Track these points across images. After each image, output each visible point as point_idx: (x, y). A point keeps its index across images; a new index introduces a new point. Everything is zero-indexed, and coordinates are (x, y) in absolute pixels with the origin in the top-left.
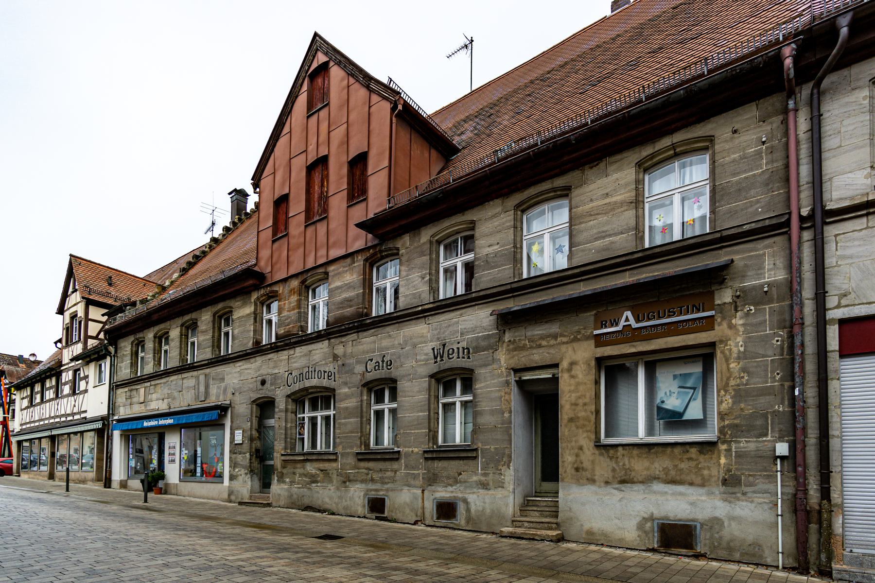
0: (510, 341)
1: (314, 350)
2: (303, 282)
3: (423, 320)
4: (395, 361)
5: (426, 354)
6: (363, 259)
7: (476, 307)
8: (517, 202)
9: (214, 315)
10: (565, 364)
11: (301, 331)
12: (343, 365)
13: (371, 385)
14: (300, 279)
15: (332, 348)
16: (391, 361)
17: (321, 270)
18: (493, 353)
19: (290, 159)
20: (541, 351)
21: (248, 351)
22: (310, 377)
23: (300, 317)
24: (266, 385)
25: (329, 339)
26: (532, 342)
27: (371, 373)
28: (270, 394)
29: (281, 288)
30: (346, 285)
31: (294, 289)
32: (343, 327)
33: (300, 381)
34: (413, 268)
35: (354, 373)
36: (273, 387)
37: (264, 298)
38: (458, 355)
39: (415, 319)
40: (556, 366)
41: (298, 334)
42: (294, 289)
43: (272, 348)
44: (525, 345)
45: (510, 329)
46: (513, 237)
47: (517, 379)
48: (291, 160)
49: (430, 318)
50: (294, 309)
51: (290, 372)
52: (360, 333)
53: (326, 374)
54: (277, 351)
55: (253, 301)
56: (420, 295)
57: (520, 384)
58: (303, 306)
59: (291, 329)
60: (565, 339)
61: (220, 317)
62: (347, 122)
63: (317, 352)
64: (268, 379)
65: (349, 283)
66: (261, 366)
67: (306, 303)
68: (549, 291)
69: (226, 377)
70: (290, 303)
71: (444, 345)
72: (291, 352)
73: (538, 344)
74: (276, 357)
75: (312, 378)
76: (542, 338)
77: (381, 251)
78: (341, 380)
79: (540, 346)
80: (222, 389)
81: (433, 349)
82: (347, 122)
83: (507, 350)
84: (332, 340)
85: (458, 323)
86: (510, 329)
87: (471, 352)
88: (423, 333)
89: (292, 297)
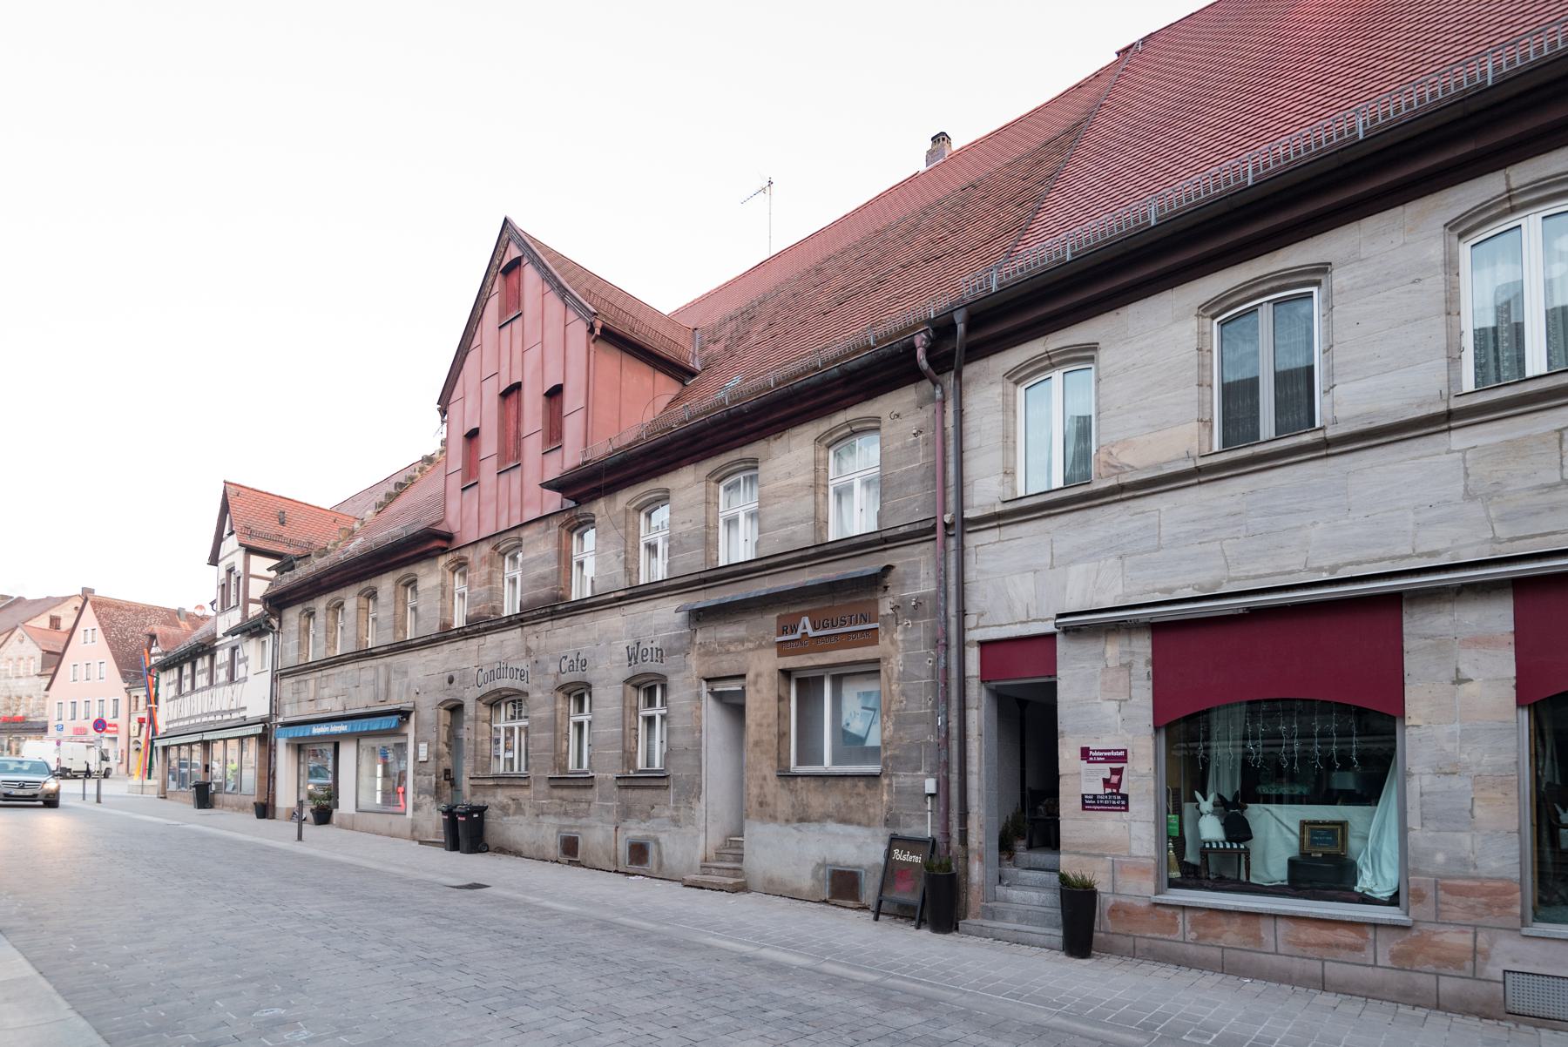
0: (701, 644)
5: (621, 654)
7: (670, 598)
10: (750, 676)
17: (514, 534)
20: (729, 658)
21: (433, 637)
27: (565, 675)
28: (458, 696)
29: (471, 554)
31: (485, 557)
36: (462, 687)
40: (743, 676)
42: (485, 557)
43: (460, 635)
47: (709, 690)
49: (625, 607)
51: (480, 668)
52: (555, 622)
53: (518, 673)
55: (440, 568)
57: (712, 693)
59: (481, 611)
60: (751, 645)
62: (542, 342)
63: (509, 643)
64: (456, 675)
65: (544, 555)
66: (448, 658)
67: (501, 576)
70: (481, 576)
71: (638, 644)
77: (577, 517)
79: (728, 652)
81: (628, 648)
83: (699, 654)
84: (525, 629)
85: (651, 616)
86: (701, 629)
89: (483, 567)
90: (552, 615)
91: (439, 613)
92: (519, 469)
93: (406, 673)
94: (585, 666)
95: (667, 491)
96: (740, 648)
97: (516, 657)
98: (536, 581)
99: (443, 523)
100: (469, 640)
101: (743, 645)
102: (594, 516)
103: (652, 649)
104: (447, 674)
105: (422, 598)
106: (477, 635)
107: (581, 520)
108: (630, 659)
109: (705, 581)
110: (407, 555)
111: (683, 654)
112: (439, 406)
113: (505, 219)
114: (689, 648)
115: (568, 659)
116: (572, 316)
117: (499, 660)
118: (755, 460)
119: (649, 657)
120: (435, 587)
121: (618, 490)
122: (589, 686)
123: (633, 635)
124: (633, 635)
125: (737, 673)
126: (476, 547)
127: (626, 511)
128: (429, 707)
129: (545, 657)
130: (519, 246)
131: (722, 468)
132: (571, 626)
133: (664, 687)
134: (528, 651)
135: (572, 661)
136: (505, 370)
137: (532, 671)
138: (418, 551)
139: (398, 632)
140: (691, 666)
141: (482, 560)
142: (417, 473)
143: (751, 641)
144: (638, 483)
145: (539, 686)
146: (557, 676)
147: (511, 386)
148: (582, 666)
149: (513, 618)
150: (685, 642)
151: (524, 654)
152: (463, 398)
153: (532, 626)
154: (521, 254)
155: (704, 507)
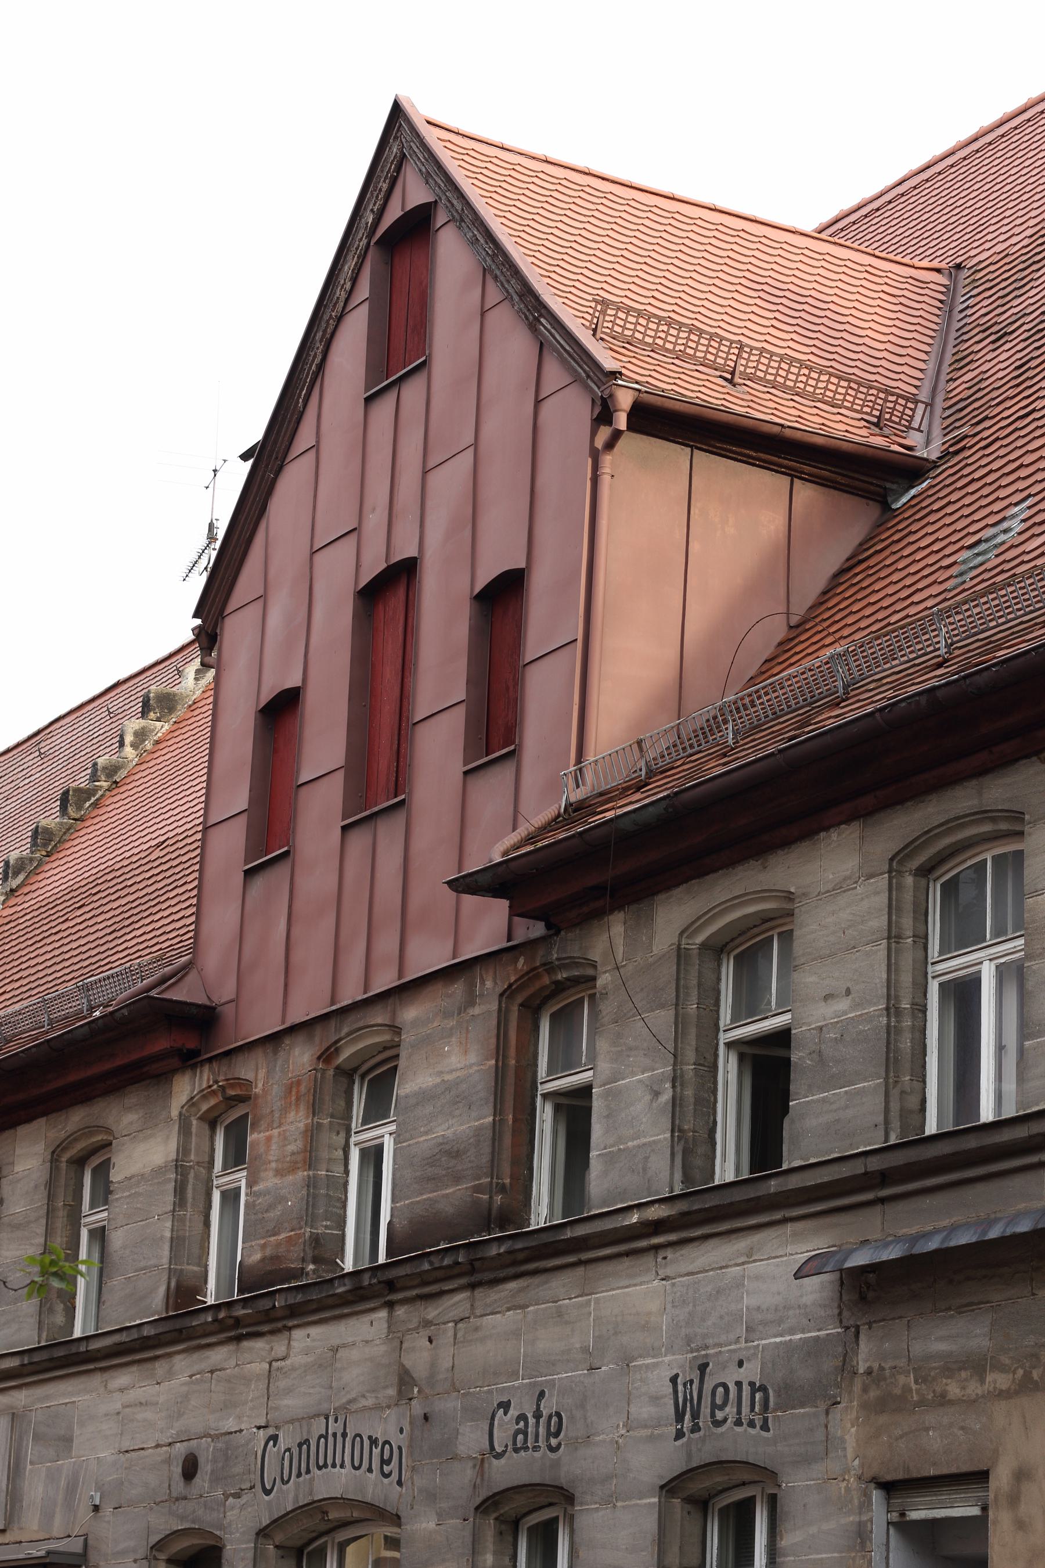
0: (869, 1372)
1: (344, 1346)
2: (327, 1056)
3: (648, 1260)
4: (572, 1418)
5: (655, 1399)
6: (499, 989)
7: (789, 1227)
8: (894, 846)
9: (54, 1159)
10: (1001, 1478)
11: (315, 1260)
12: (426, 1418)
13: (507, 1509)
14: (322, 1039)
15: (397, 1343)
16: (559, 1415)
17: (379, 1017)
18: (827, 1413)
19: (313, 553)
20: (945, 1420)
21: (146, 1332)
22: (329, 1462)
23: (311, 1201)
24: (197, 1480)
25: (390, 1305)
26: (925, 1381)
27: (503, 1461)
28: (207, 1519)
29: (262, 1073)
30: (448, 1087)
31: (299, 1083)
32: (426, 1266)
33: (299, 1475)
34: (630, 1049)
35: (455, 1457)
36: (219, 1493)
37: (213, 1102)
38: (739, 1412)
39: (628, 1254)
40: (980, 1477)
41: (301, 1273)
42: (299, 1083)
43: (220, 1326)
44: (906, 1389)
45: (870, 1325)
46: (885, 976)
47: (894, 1516)
48: (319, 558)
49: (669, 1253)
50: (293, 1169)
51: (271, 1431)
52: (479, 1293)
53: (376, 1451)
54: (239, 1339)
55: (175, 1113)
56: (647, 1158)
57: (904, 1527)
58: (324, 1154)
59: (282, 1250)
60: (1001, 1380)
61: (80, 1162)
62: (476, 444)
63: (355, 1354)
64: (206, 1452)
65: (457, 1083)
66: (186, 1397)
67: (341, 1139)
68: (969, 1193)
69: (77, 1431)
70: (284, 1139)
71: (703, 1368)
72: (279, 1346)
73: (938, 1389)
74: (233, 1362)
75: (334, 1466)
76: (951, 1366)
77: (549, 968)
78: (420, 1482)
79: (943, 1401)
80: (63, 1483)
81: (674, 1380)
82: (476, 444)
83: (864, 1406)
84: (400, 1312)
85: (738, 1283)
86: (870, 1325)
87: (771, 1404)
88: (649, 1314)
89: (291, 1116)
90: (473, 1271)
91: (166, 1252)
92: (400, 818)
93: (67, 1440)
94: (557, 1435)
95: (789, 897)
96: (974, 1388)
97: (369, 1402)
98: (432, 1161)
99: (192, 977)
100: (246, 1344)
101: (982, 1381)
102: (595, 967)
103: (739, 1384)
104: (180, 1449)
105: (121, 1201)
106: (265, 1328)
107: (562, 975)
108: (679, 1417)
109: (884, 1178)
110: (90, 1072)
111: (822, 1407)
112: (198, 622)
113: (397, 112)
114: (838, 1386)
115: (513, 1413)
116: (554, 374)
117: (325, 1407)
118: (1017, 816)
119: (730, 1410)
120: (159, 1171)
121: (655, 893)
122: (569, 1498)
123: (689, 1340)
124: (689, 1340)
125: (965, 1468)
126: (275, 1052)
127: (681, 955)
128: (123, 1553)
129: (449, 1405)
130: (427, 177)
131: (929, 836)
132: (523, 1307)
133: (773, 1502)
134: (405, 1380)
135: (522, 1417)
136: (375, 521)
137: (410, 1446)
138: (118, 1062)
139: (51, 1311)
140: (843, 1440)
141: (289, 1089)
142: (129, 751)
143: (1002, 1369)
144: (715, 870)
145: (431, 1496)
146: (481, 1464)
147: (388, 567)
148: (549, 1434)
149: (366, 1280)
150: (829, 1364)
151: (392, 1392)
152: (263, 598)
153: (420, 1305)
154: (432, 200)
155: (883, 954)
